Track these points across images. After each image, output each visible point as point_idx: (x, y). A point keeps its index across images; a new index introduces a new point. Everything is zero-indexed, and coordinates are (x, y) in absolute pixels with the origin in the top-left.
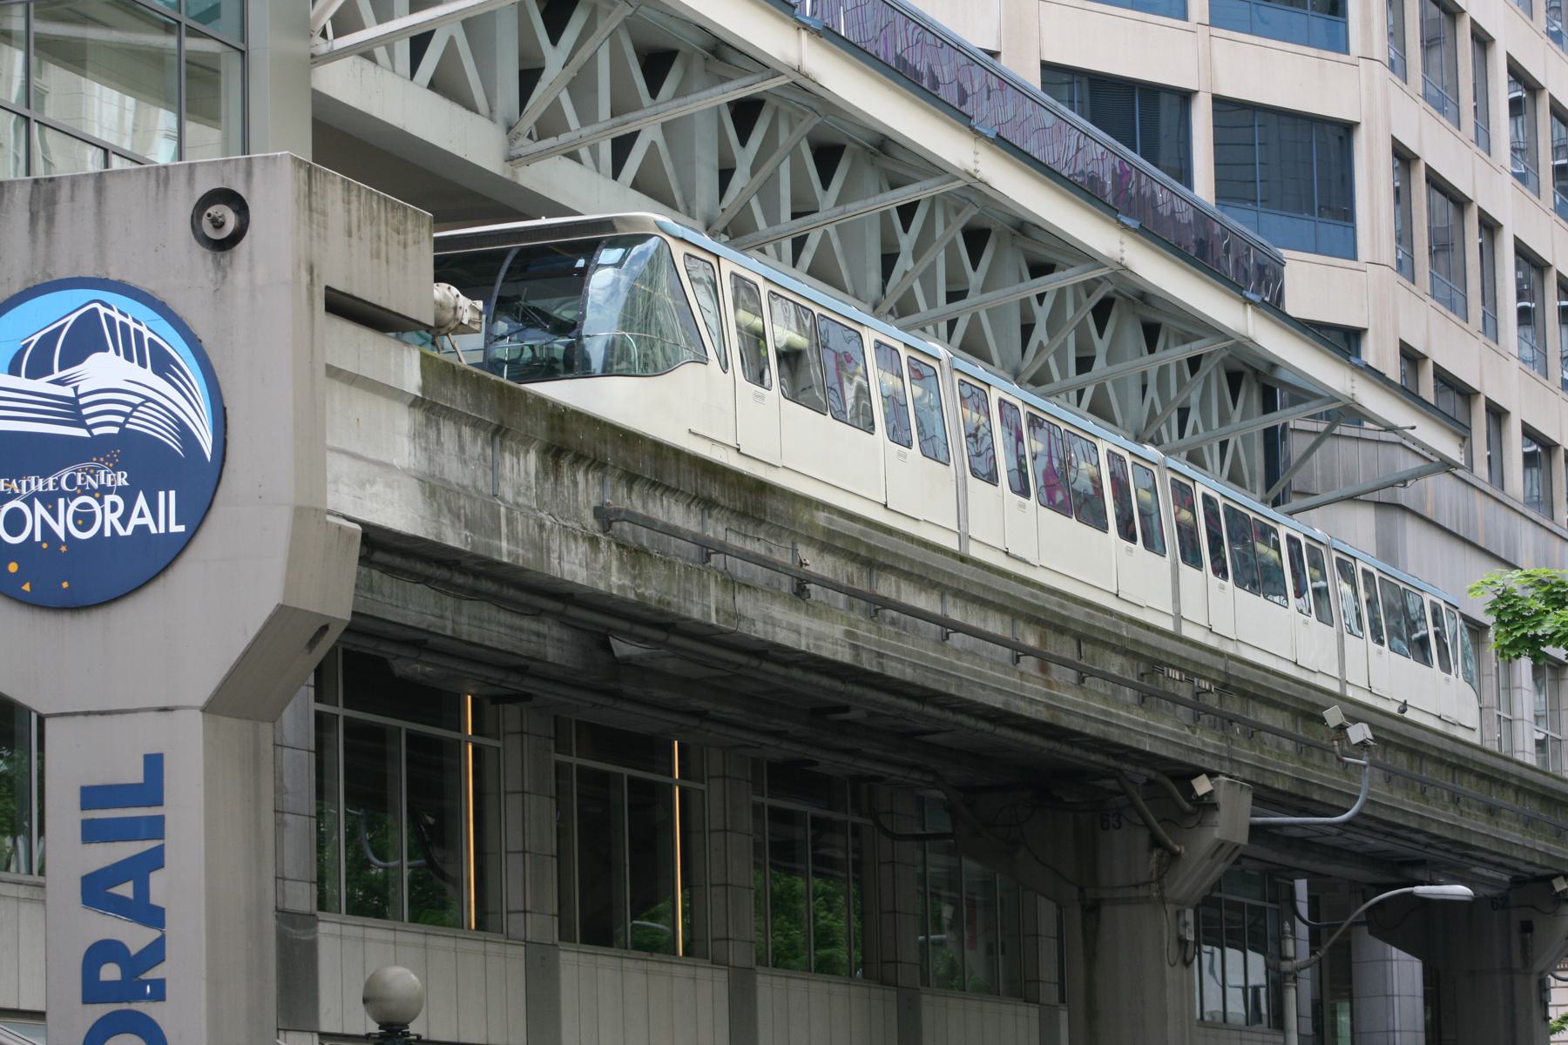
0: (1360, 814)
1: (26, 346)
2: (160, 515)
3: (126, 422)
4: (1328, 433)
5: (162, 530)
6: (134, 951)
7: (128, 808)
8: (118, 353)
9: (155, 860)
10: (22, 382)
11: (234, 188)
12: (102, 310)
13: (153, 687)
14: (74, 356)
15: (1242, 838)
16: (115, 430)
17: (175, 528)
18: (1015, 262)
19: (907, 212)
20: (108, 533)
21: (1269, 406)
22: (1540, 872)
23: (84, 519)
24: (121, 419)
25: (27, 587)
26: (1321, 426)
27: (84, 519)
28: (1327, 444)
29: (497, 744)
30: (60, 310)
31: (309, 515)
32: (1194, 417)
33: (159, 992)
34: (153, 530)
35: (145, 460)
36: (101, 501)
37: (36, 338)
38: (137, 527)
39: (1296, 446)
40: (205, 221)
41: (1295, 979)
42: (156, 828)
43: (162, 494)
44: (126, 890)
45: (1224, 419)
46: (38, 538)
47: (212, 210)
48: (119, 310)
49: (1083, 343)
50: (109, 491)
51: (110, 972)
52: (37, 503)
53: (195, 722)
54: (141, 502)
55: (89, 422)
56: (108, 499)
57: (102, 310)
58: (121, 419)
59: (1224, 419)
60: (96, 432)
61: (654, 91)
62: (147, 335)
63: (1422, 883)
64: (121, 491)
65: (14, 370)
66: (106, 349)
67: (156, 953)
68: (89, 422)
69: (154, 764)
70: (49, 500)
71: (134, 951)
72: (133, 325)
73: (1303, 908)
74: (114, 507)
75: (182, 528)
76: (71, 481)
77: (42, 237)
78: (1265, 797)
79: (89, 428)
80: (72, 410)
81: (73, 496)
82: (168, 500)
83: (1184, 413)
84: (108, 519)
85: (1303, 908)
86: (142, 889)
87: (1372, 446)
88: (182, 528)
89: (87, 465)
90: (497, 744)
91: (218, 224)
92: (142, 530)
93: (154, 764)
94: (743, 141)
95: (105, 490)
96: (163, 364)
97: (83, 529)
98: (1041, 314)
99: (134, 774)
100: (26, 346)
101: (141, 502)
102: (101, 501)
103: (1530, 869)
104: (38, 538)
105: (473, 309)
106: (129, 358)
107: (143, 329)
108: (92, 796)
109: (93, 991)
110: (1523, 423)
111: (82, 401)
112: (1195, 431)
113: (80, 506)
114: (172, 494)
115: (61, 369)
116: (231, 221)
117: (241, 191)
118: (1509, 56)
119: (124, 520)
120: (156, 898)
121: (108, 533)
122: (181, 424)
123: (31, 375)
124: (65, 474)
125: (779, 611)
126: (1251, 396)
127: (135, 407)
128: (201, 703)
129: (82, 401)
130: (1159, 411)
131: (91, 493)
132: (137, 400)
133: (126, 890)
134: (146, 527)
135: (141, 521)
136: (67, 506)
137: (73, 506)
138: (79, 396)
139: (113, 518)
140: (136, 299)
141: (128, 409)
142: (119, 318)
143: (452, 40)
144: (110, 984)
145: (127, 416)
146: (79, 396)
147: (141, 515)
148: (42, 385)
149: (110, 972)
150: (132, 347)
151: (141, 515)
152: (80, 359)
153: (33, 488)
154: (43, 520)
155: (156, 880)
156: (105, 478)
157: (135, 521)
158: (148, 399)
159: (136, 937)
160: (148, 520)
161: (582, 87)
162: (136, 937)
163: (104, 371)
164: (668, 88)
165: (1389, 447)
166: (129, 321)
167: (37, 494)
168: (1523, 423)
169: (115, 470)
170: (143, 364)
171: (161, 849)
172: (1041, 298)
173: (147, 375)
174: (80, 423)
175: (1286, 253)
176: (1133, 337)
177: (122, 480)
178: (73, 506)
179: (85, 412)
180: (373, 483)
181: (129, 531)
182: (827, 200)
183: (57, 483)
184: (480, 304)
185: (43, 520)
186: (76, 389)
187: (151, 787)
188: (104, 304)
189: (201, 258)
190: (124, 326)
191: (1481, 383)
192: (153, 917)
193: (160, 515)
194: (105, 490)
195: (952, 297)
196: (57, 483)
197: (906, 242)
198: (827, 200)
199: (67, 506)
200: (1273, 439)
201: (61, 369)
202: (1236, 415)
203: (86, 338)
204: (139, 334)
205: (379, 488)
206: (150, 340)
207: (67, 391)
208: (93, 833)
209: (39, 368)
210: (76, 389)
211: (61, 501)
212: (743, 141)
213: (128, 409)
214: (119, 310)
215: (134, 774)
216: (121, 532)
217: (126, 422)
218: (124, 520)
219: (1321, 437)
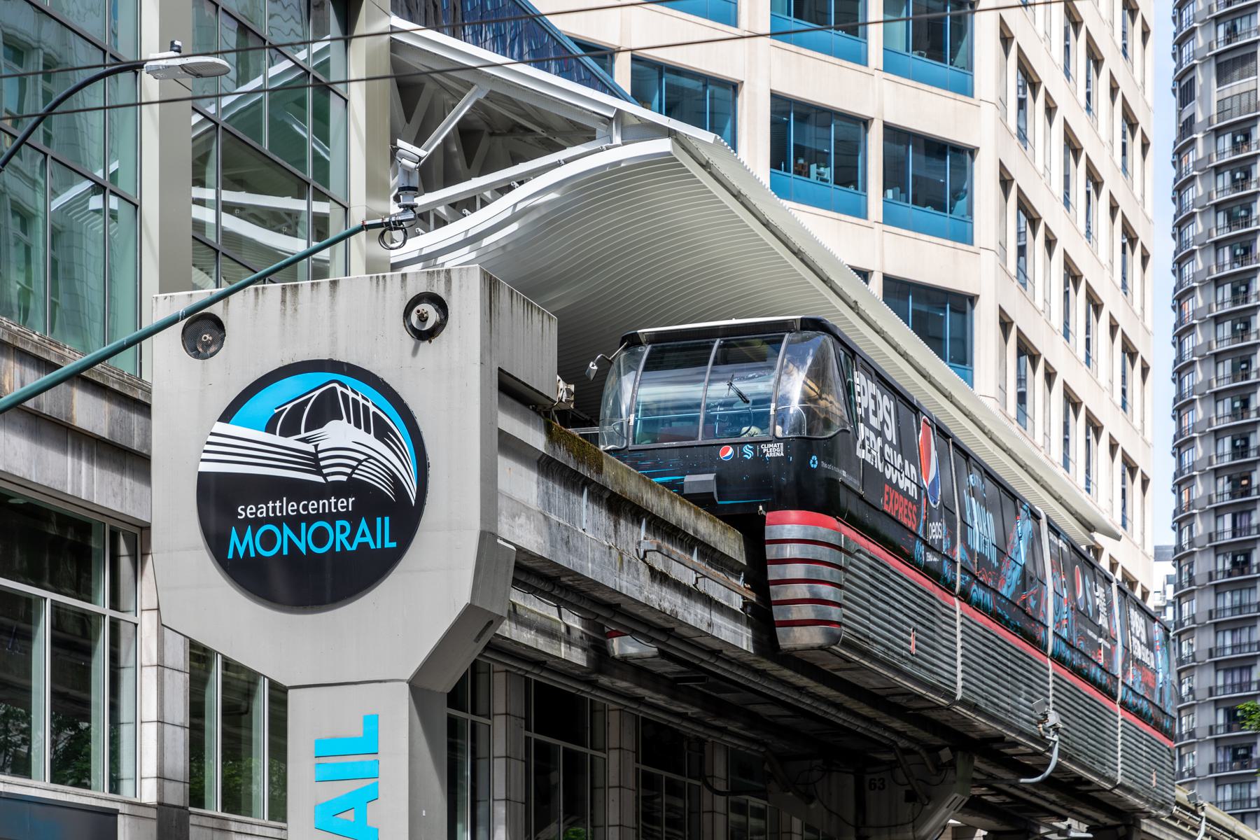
1: (277, 416)
2: (380, 536)
3: (353, 472)
5: (379, 546)
10: (276, 439)
11: (435, 291)
12: (339, 389)
14: (317, 420)
16: (344, 478)
17: (388, 545)
20: (338, 549)
23: (320, 537)
24: (349, 471)
27: (320, 537)
34: (372, 546)
37: (289, 406)
40: (429, 325)
43: (379, 520)
46: (285, 552)
47: (421, 307)
54: (363, 525)
55: (325, 471)
56: (339, 523)
57: (339, 389)
58: (349, 471)
60: (330, 479)
62: (372, 409)
65: (270, 428)
66: (341, 418)
68: (325, 471)
72: (362, 401)
74: (343, 529)
75: (394, 545)
77: (381, 292)
79: (325, 476)
80: (313, 462)
82: (384, 524)
84: (338, 538)
88: (394, 545)
91: (423, 318)
93: (372, 722)
96: (382, 432)
97: (319, 545)
101: (363, 525)
104: (285, 552)
106: (358, 425)
107: (369, 405)
111: (321, 456)
114: (387, 519)
116: (433, 316)
117: (442, 294)
119: (351, 539)
121: (338, 549)
122: (394, 477)
123: (285, 433)
127: (360, 462)
128: (408, 677)
129: (321, 456)
132: (362, 457)
134: (367, 544)
135: (364, 540)
138: (318, 452)
139: (341, 538)
140: (284, 720)
141: (355, 464)
142: (351, 395)
145: (354, 468)
147: (363, 535)
148: (291, 442)
150: (360, 417)
151: (363, 535)
152: (321, 425)
157: (358, 539)
158: (370, 457)
160: (369, 539)
163: (339, 434)
166: (359, 398)
170: (367, 430)
173: (370, 439)
174: (318, 471)
181: (354, 547)
186: (316, 446)
189: (409, 341)
190: (355, 402)
193: (380, 536)
203: (326, 409)
204: (366, 409)
207: (310, 448)
209: (290, 428)
210: (316, 446)
211: (303, 525)
213: (355, 464)
215: (355, 729)
216: (348, 548)
217: (353, 472)
218: (351, 539)
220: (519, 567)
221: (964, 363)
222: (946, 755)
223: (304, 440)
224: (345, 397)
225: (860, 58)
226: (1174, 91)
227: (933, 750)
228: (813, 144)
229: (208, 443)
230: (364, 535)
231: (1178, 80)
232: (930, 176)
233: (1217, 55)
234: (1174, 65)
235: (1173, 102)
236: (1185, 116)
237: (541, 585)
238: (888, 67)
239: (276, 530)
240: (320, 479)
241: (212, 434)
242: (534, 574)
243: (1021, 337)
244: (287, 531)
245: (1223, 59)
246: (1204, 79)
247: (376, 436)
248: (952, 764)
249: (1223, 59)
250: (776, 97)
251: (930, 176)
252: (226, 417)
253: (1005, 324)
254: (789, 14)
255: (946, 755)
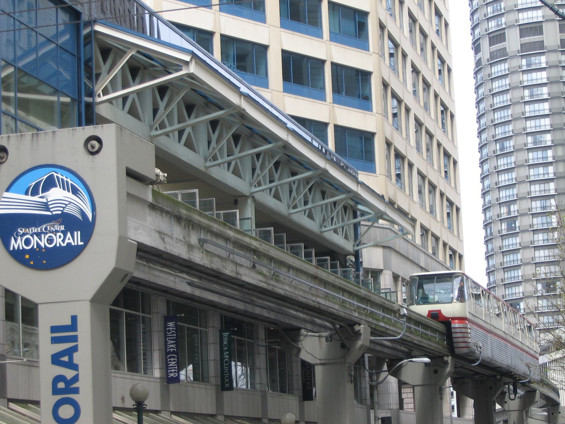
0: (400, 338)
2: (75, 239)
4: (372, 226)
6: (69, 378)
7: (65, 333)
8: (60, 188)
9: (75, 349)
10: (29, 197)
12: (55, 175)
13: (70, 295)
14: (45, 189)
15: (368, 344)
16: (60, 212)
17: (81, 243)
18: (287, 172)
19: (258, 155)
21: (355, 216)
22: (440, 355)
23: (50, 241)
24: (62, 209)
25: (32, 263)
26: (369, 224)
27: (50, 241)
28: (372, 229)
29: (150, 316)
30: (43, 176)
31: (123, 240)
32: (335, 219)
33: (76, 391)
34: (73, 244)
35: (70, 222)
36: (56, 235)
37: (34, 183)
38: (68, 244)
39: (362, 229)
40: (89, 146)
41: (377, 387)
42: (74, 339)
43: (76, 233)
44: (66, 359)
45: (343, 220)
48: (58, 175)
49: (305, 196)
50: (58, 232)
51: (61, 385)
52: (35, 236)
53: (88, 304)
54: (69, 235)
55: (51, 210)
56: (58, 234)
58: (62, 209)
59: (343, 220)
60: (54, 213)
61: (189, 116)
62: (70, 182)
63: (415, 357)
64: (62, 232)
65: (26, 193)
66: (56, 186)
67: (76, 379)
68: (51, 210)
69: (74, 319)
70: (39, 235)
71: (69, 378)
72: (65, 179)
73: (367, 367)
74: (60, 237)
75: (82, 243)
76: (46, 229)
78: (375, 332)
79: (51, 212)
80: (46, 206)
81: (46, 234)
83: (332, 219)
84: (58, 240)
85: (367, 367)
86: (71, 358)
87: (381, 229)
88: (82, 243)
89: (51, 224)
90: (150, 316)
91: (93, 147)
92: (69, 244)
93: (74, 319)
94: (214, 132)
95: (57, 231)
96: (75, 191)
98: (294, 187)
99: (68, 322)
100: (30, 186)
101: (69, 235)
102: (56, 235)
103: (438, 354)
104: (35, 247)
105: (164, 176)
106: (64, 189)
108: (54, 329)
109: (56, 391)
110: (421, 223)
111: (49, 203)
112: (335, 224)
113: (49, 237)
114: (79, 232)
115: (42, 193)
118: (415, 114)
119: (63, 241)
120: (75, 361)
122: (81, 210)
124: (44, 226)
125: (247, 272)
126: (350, 213)
127: (66, 205)
129: (49, 203)
130: (326, 218)
131: (52, 232)
132: (67, 203)
133: (66, 359)
136: (45, 237)
137: (47, 236)
138: (48, 202)
139: (60, 240)
141: (64, 206)
143: (134, 99)
144: (61, 389)
145: (64, 208)
146: (48, 202)
147: (69, 239)
148: (36, 198)
149: (61, 385)
151: (69, 239)
153: (34, 231)
154: (37, 242)
155: (75, 355)
156: (57, 227)
157: (67, 241)
159: (69, 374)
160: (71, 241)
161: (169, 116)
162: (69, 374)
163: (56, 194)
164: (193, 115)
165: (386, 230)
166: (64, 178)
167: (35, 233)
168: (421, 223)
169: (60, 225)
170: (68, 191)
171: (77, 346)
172: (294, 183)
173: (70, 195)
175: (359, 172)
176: (319, 195)
177: (62, 228)
178: (47, 236)
179: (50, 207)
180: (139, 229)
181: (65, 245)
182: (236, 151)
183: (41, 229)
184: (166, 175)
185: (37, 242)
187: (73, 326)
188: (56, 172)
190: (62, 180)
191: (409, 210)
192: (75, 367)
193: (75, 239)
194: (57, 231)
195: (271, 182)
196: (41, 229)
197: (258, 165)
198: (236, 151)
199: (45, 237)
200: (356, 226)
201: (42, 193)
202: (346, 219)
203: (50, 184)
205: (141, 231)
206: (71, 184)
207: (44, 200)
208: (55, 340)
209: (35, 192)
211: (43, 235)
212: (214, 132)
213: (64, 206)
214: (58, 175)
215: (68, 322)
216: (63, 245)
218: (63, 241)
219: (370, 227)
220: (138, 250)
221: (372, 161)
222: (498, 377)
223: (42, 197)
224: (57, 177)
225: (320, 35)
226: (472, 48)
227: (495, 376)
228: (300, 72)
229: (2, 201)
230: (69, 240)
231: (474, 43)
232: (353, 85)
233: (489, 34)
234: (472, 38)
235: (472, 52)
236: (477, 58)
237: (153, 258)
238: (331, 40)
239: (31, 237)
240: (49, 213)
241: (4, 198)
242: (145, 253)
243: (396, 150)
244: (36, 238)
245: (491, 35)
246: (485, 44)
247: (73, 193)
248: (500, 380)
249: (491, 35)
250: (283, 51)
251: (353, 85)
252: (8, 190)
253: (389, 144)
254: (288, 18)
255: (498, 377)
